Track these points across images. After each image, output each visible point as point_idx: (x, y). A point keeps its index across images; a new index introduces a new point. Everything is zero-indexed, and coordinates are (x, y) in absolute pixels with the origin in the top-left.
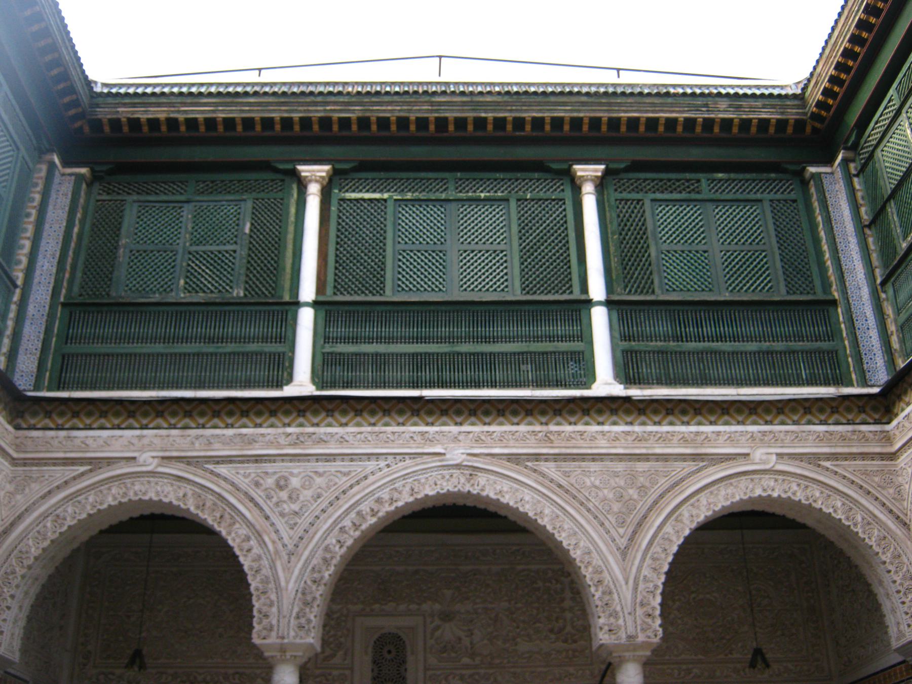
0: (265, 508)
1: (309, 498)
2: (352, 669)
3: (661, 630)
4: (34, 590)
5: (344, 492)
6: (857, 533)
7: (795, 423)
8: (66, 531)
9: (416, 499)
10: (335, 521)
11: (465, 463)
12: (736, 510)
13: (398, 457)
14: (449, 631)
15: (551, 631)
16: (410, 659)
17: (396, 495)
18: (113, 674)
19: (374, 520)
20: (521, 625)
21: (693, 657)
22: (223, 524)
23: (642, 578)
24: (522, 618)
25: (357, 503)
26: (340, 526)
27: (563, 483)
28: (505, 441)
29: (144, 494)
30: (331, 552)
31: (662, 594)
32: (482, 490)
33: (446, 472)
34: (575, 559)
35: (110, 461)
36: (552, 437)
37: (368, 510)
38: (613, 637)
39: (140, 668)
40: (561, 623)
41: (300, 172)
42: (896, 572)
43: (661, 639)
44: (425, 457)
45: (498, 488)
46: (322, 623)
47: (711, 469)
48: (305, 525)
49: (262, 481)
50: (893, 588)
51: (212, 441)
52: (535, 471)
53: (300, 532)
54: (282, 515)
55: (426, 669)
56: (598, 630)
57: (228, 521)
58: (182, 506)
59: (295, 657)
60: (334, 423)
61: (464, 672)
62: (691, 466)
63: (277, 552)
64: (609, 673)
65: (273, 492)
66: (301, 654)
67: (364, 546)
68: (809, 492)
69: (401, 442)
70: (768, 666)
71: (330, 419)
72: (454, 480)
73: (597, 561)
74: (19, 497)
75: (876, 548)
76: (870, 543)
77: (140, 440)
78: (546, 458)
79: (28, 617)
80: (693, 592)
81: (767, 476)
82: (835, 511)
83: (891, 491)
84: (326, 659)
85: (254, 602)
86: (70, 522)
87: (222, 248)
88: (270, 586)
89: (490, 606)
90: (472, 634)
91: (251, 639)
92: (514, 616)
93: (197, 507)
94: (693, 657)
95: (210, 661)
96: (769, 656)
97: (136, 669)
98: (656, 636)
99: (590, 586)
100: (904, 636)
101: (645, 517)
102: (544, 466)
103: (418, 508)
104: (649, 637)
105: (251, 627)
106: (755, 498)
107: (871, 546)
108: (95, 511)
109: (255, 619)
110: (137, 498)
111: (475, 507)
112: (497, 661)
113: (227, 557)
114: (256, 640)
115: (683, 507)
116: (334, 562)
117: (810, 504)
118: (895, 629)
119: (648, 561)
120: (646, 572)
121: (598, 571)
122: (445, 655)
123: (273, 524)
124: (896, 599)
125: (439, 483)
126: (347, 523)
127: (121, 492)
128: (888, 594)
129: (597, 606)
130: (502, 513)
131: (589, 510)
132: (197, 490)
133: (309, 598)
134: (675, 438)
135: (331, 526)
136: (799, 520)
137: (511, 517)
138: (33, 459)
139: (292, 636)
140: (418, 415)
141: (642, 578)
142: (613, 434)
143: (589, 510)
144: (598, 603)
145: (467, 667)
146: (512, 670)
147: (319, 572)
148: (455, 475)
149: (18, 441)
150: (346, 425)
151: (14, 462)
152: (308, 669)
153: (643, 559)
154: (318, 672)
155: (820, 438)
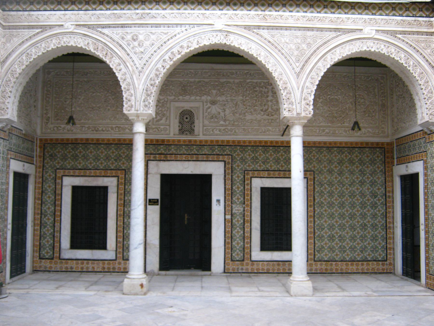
0: (127, 49)
1: (148, 45)
2: (169, 126)
3: (312, 111)
4: (21, 89)
5: (165, 43)
6: (410, 70)
7: (387, 15)
8: (33, 61)
9: (200, 46)
10: (161, 56)
11: (223, 30)
12: (353, 57)
13: (191, 26)
14: (214, 109)
15: (262, 110)
16: (196, 121)
17: (190, 44)
18: (60, 127)
19: (179, 56)
20: (248, 107)
21: (326, 124)
22: (107, 58)
23: (305, 87)
24: (248, 104)
25: (171, 48)
26: (163, 59)
27: (271, 40)
28: (243, 19)
29: (68, 43)
30: (159, 71)
31: (315, 95)
32: (232, 43)
33: (215, 34)
34: (275, 77)
35: (51, 27)
36: (266, 18)
37: (177, 51)
38: (290, 113)
39: (73, 124)
40: (266, 106)
42: (425, 89)
43: (312, 115)
44: (204, 26)
45: (239, 42)
46: (155, 104)
47: (343, 36)
48: (147, 58)
49: (125, 37)
50: (422, 97)
51: (100, 17)
52: (258, 34)
53: (144, 62)
54: (135, 53)
55: (204, 126)
56: (283, 110)
57: (110, 56)
58: (87, 49)
59: (143, 119)
60: (160, 8)
61: (221, 128)
62: (333, 34)
63: (133, 71)
64: (287, 130)
65: (130, 42)
66: (146, 118)
67: (175, 69)
68: (389, 50)
69: (193, 18)
70: (360, 129)
71: (157, 6)
72: (218, 38)
73: (285, 78)
74: (8, 45)
75: (417, 78)
76: (415, 75)
77: (64, 16)
78: (263, 27)
79: (19, 101)
80: (329, 95)
81: (370, 41)
82: (400, 59)
83: (429, 51)
84: (158, 121)
85: (124, 94)
86: (34, 57)
88: (131, 87)
89: (234, 98)
90: (225, 111)
91: (123, 111)
92: (245, 103)
93: (95, 49)
94: (326, 124)
95: (104, 121)
96: (361, 125)
97: (71, 125)
98: (310, 114)
99: (281, 90)
100: (424, 118)
101: (309, 58)
102: (261, 32)
103: (200, 51)
104: (307, 114)
105: (123, 106)
106: (363, 51)
107: (415, 77)
108: (46, 51)
109: (124, 102)
110: (65, 45)
111: (228, 51)
112: (236, 123)
113: (110, 74)
114: (125, 112)
115: (328, 54)
116: (161, 76)
117: (389, 55)
118: (421, 116)
119: (309, 79)
120: (308, 84)
121: (285, 83)
122: (212, 120)
123: (131, 58)
124: (423, 102)
125: (210, 39)
126: (167, 57)
127: (57, 42)
128: (420, 100)
129: (284, 99)
130: (241, 54)
131: (282, 54)
132: (94, 41)
133: (149, 93)
134: (327, 20)
135: (159, 59)
136: (383, 63)
137: (245, 57)
138: (13, 26)
139: (142, 110)
140: (201, 5)
141: (305, 87)
142: (297, 17)
143: (282, 54)
144: (285, 98)
145: (222, 125)
146: (243, 127)
147: (154, 80)
148: (218, 35)
149: (5, 17)
150: (166, 9)
151: (4, 27)
152: (149, 125)
153: (307, 78)
154: (154, 127)
155: (398, 23)
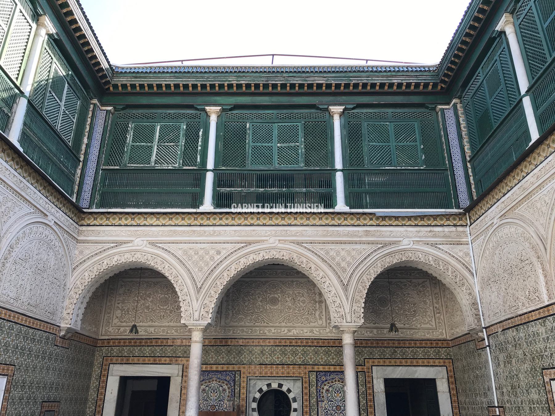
41: (330, 109)
87: (264, 145)
